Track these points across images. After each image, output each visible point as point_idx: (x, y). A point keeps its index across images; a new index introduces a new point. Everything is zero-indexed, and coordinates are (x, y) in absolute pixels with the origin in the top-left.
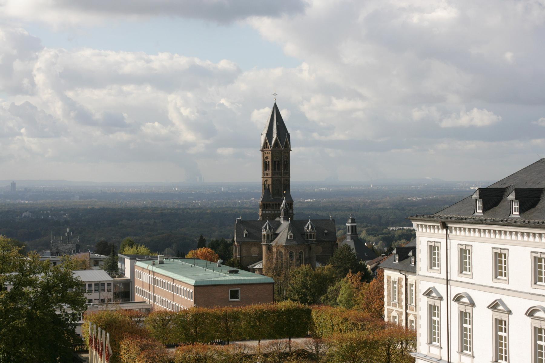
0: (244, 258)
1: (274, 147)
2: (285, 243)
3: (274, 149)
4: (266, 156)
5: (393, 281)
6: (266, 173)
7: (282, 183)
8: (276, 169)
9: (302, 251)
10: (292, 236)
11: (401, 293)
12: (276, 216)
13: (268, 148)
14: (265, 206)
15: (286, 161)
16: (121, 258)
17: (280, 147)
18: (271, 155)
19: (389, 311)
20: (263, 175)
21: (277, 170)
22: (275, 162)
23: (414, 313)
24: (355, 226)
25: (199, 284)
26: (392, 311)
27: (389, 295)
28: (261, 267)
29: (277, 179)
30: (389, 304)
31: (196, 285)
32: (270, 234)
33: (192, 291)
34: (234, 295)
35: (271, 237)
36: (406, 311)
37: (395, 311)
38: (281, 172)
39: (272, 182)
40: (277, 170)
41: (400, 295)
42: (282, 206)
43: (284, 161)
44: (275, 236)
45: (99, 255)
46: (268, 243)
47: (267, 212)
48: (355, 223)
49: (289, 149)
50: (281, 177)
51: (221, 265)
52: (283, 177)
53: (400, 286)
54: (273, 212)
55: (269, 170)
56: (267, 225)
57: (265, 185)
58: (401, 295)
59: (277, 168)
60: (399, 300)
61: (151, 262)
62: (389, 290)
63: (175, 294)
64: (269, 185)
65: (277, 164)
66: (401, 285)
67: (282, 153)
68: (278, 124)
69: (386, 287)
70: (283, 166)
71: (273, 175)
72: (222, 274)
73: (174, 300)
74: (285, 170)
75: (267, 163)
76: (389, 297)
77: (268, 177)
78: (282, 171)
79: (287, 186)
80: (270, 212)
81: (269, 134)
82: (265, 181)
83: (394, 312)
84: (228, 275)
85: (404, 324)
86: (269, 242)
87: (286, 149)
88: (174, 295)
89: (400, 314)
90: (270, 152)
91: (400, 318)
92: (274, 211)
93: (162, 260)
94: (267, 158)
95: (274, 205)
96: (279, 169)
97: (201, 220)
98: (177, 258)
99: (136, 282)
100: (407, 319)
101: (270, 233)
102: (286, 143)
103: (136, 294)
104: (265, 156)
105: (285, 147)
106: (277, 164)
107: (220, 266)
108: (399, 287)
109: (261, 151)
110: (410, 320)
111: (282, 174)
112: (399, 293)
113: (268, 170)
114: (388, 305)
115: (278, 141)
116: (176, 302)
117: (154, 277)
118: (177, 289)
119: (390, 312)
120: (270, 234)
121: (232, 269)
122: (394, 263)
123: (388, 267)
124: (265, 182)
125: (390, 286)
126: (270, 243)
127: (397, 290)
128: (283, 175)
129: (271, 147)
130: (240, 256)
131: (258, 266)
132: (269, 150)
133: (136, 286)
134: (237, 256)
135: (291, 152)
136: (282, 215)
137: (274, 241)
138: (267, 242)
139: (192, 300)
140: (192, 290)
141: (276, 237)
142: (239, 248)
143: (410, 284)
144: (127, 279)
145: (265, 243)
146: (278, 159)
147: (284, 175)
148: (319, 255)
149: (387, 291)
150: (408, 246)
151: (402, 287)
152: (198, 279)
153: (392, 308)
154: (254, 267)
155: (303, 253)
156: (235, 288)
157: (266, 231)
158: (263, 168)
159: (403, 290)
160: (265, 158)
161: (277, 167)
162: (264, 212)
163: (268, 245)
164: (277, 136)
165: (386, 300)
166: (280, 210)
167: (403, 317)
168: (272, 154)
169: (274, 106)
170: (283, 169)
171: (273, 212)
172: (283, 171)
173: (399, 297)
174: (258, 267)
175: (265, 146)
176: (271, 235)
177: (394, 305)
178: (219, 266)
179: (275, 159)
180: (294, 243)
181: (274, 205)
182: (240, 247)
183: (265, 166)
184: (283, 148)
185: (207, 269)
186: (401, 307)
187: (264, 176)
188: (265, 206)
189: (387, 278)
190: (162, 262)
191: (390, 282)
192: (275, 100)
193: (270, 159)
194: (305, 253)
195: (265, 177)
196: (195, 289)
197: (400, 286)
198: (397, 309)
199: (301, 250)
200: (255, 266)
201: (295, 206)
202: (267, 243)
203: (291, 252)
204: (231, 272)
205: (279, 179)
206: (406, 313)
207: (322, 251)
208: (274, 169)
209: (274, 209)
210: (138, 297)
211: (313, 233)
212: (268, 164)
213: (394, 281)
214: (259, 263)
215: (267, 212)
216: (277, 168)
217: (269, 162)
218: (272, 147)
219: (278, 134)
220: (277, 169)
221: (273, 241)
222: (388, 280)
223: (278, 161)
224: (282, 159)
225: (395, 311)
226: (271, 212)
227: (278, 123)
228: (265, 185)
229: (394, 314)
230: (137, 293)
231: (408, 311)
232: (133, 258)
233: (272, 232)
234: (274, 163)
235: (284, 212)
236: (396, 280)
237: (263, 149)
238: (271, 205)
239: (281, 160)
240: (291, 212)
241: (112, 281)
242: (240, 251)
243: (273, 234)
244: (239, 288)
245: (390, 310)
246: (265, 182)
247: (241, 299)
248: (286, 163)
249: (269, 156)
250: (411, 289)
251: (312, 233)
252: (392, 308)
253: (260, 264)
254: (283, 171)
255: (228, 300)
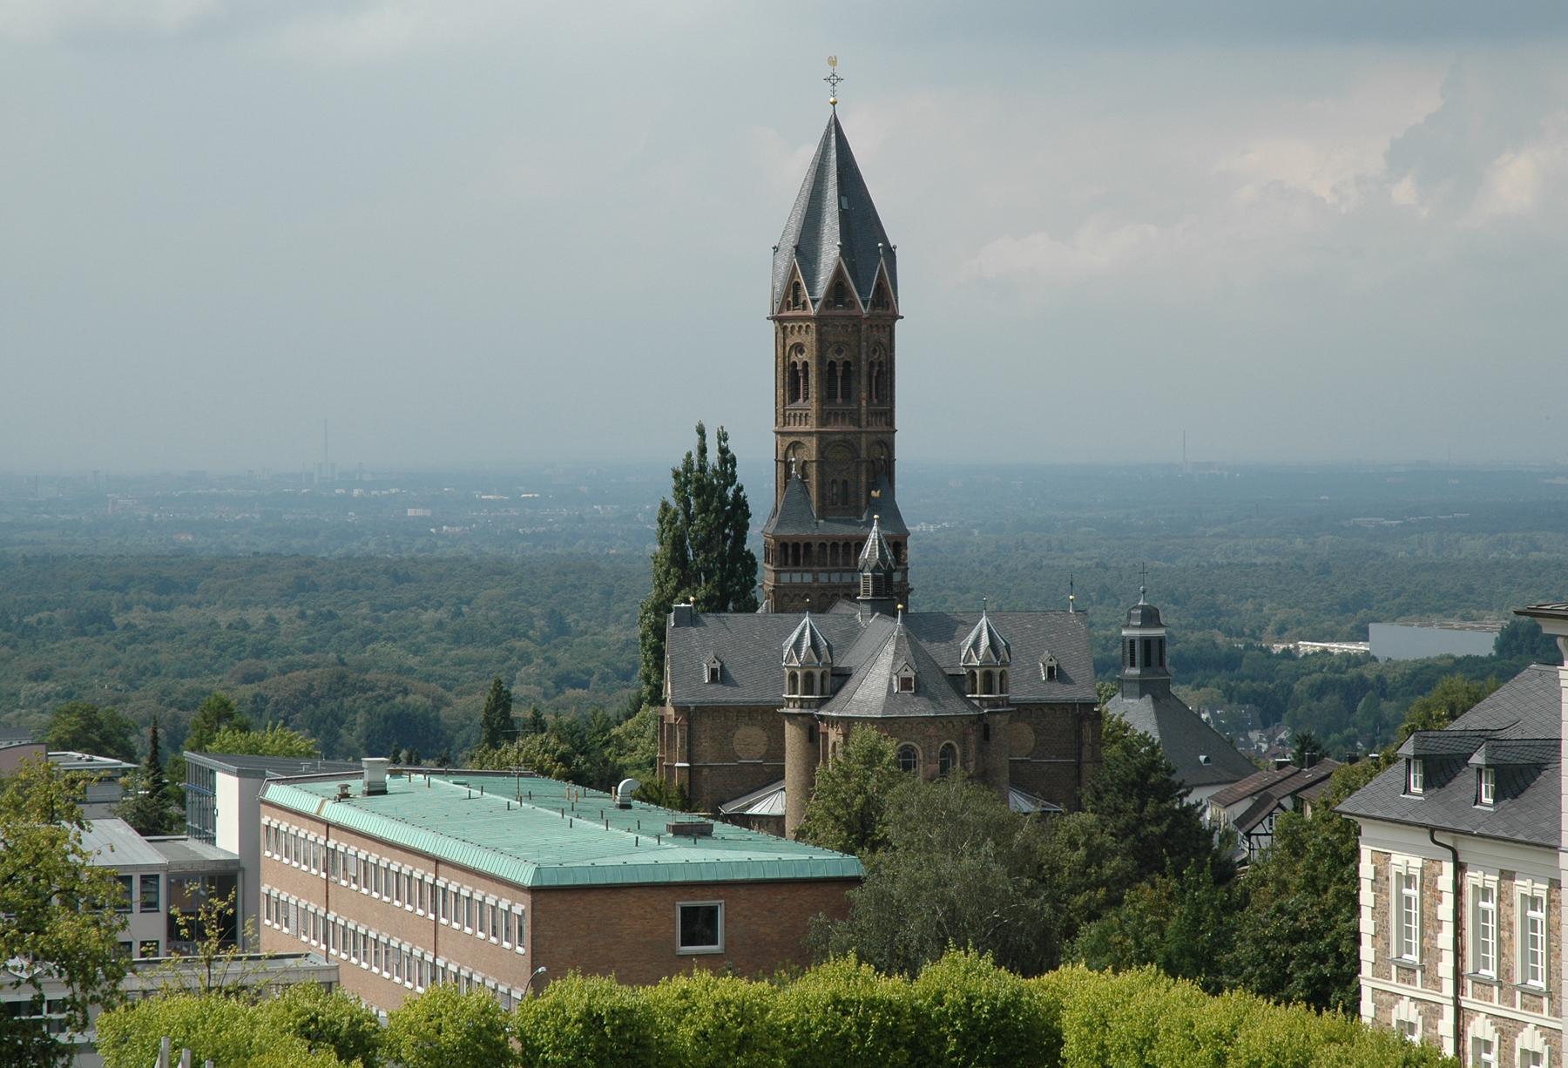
0: (705, 772)
1: (829, 301)
2: (880, 711)
3: (828, 313)
4: (793, 339)
5: (1399, 874)
6: (795, 414)
7: (863, 454)
8: (836, 397)
9: (954, 743)
10: (910, 679)
11: (1436, 924)
12: (837, 595)
13: (805, 307)
14: (790, 552)
15: (880, 364)
16: (200, 769)
17: (852, 304)
18: (814, 335)
19: (1381, 1002)
20: (780, 420)
21: (839, 400)
22: (832, 364)
23: (1545, 1018)
24: (1161, 641)
25: (554, 883)
26: (1397, 1002)
27: (1380, 933)
28: (778, 810)
29: (838, 437)
30: (1380, 970)
31: (537, 884)
32: (817, 673)
33: (523, 911)
34: (698, 926)
35: (822, 685)
36: (1456, 1000)
37: (1531, 1027)
38: (859, 410)
39: (821, 451)
40: (839, 400)
41: (1430, 932)
42: (866, 554)
43: (871, 365)
44: (836, 680)
45: (87, 756)
46: (809, 708)
47: (797, 578)
48: (1160, 625)
49: (890, 311)
50: (857, 429)
51: (635, 803)
52: (866, 432)
53: (1431, 896)
54: (823, 578)
55: (806, 398)
56: (802, 634)
57: (788, 465)
58: (1436, 933)
59: (839, 394)
60: (1429, 953)
61: (334, 786)
62: (1380, 911)
63: (443, 921)
64: (804, 466)
65: (839, 374)
66: (1435, 890)
67: (864, 327)
68: (845, 206)
69: (1366, 897)
70: (864, 381)
71: (823, 419)
72: (644, 838)
73: (440, 948)
74: (875, 401)
75: (797, 372)
76: (1381, 942)
77: (802, 428)
78: (861, 404)
79: (883, 469)
80: (808, 578)
81: (806, 250)
82: (788, 448)
83: (1405, 1002)
84: (669, 846)
85: (1449, 1050)
86: (813, 704)
87: (879, 311)
88: (440, 929)
89: (1432, 1012)
90: (813, 326)
91: (1430, 1030)
92: (826, 575)
93: (376, 777)
94: (799, 348)
95: (828, 548)
96: (847, 395)
97: (465, 609)
98: (441, 773)
99: (265, 873)
100: (1459, 1034)
101: (818, 666)
102: (879, 285)
103: (267, 922)
104: (790, 342)
105: (874, 305)
106: (839, 374)
107: (629, 807)
108: (1428, 900)
109: (774, 319)
110: (1476, 1040)
111: (864, 417)
112: (1430, 924)
113: (801, 400)
114: (1376, 974)
115: (845, 280)
116: (446, 955)
117: (331, 844)
118: (451, 900)
119: (1386, 1001)
120: (817, 673)
121: (684, 818)
122: (1477, 807)
123: (1378, 814)
124: (791, 452)
125: (1387, 894)
126: (819, 707)
127: (1415, 912)
128: (864, 423)
129: (814, 302)
130: (687, 765)
131: (770, 804)
132: (808, 318)
133: (264, 889)
134: (677, 764)
135: (898, 323)
136: (866, 591)
137: (836, 698)
138: (806, 704)
139: (520, 950)
140: (523, 907)
141: (842, 685)
142: (686, 728)
143: (1475, 887)
144: (222, 857)
145: (796, 711)
146: (843, 356)
147: (868, 422)
148: (1022, 761)
149: (1373, 917)
150: (1462, 727)
151: (1441, 900)
152: (548, 860)
153: (1393, 985)
154: (748, 812)
155: (958, 752)
156: (702, 898)
157: (798, 656)
158: (781, 391)
159: (1446, 910)
160: (788, 349)
161: (842, 389)
162: (785, 578)
163: (806, 719)
164: (841, 254)
165: (1367, 952)
166: (856, 571)
167: (1446, 1026)
168: (819, 331)
169: (827, 137)
170: (864, 395)
171: (823, 578)
172: (864, 403)
173: (1425, 940)
174: (765, 812)
175: (790, 299)
176: (823, 676)
177: (1407, 972)
178: (625, 806)
179: (831, 356)
180: (919, 711)
181: (828, 548)
182: (690, 727)
183: (792, 381)
184: (865, 307)
185: (578, 817)
186: (1437, 983)
187: (785, 425)
188: (790, 552)
189: (1372, 862)
190: (377, 790)
191: (1388, 879)
192: (834, 104)
193: (809, 356)
194: (965, 753)
195: (787, 429)
196: (533, 903)
197: (1431, 896)
198: (1417, 990)
199: (949, 741)
200: (750, 806)
201: (912, 553)
202: (804, 711)
203: (913, 749)
204: (679, 831)
205: (849, 437)
206: (1458, 1010)
207: (1032, 744)
208: (827, 396)
209: (825, 565)
210: (272, 933)
211: (1000, 670)
212: (801, 374)
213: (1481, 886)
214: (776, 792)
215: (797, 578)
216: (839, 394)
217: (806, 364)
218: (818, 305)
219: (847, 249)
220: (842, 397)
221: (829, 699)
222: (1375, 868)
223: (847, 364)
224: (864, 356)
225: (1531, 1027)
226: (816, 580)
227: (844, 200)
228: (788, 465)
229: (1405, 1011)
230: (268, 918)
231: (1467, 1001)
232: (252, 774)
233: (824, 664)
234: (829, 373)
235: (875, 579)
236: (1411, 871)
237: (780, 311)
238: (815, 549)
239: (858, 360)
240: (897, 577)
241: (160, 866)
242: (689, 744)
243: (829, 670)
244: (721, 898)
245: (1384, 997)
246: (791, 452)
247: (729, 943)
248: (878, 371)
249: (809, 339)
250: (1478, 907)
251: (997, 666)
252: (1393, 985)
253: (774, 798)
254: (864, 403)
255: (674, 951)
